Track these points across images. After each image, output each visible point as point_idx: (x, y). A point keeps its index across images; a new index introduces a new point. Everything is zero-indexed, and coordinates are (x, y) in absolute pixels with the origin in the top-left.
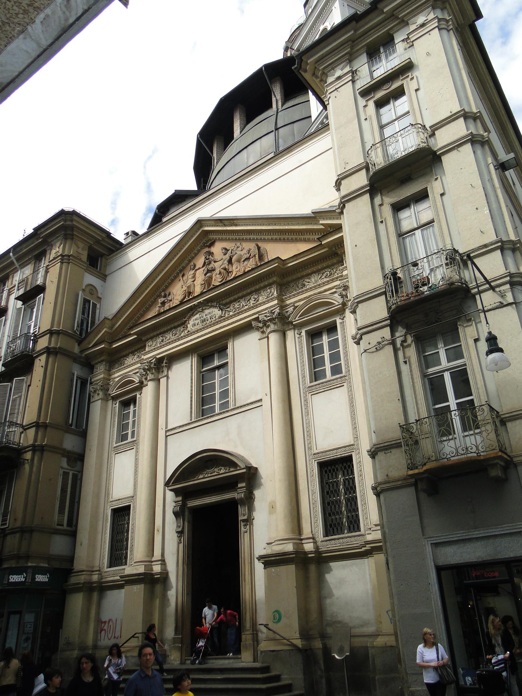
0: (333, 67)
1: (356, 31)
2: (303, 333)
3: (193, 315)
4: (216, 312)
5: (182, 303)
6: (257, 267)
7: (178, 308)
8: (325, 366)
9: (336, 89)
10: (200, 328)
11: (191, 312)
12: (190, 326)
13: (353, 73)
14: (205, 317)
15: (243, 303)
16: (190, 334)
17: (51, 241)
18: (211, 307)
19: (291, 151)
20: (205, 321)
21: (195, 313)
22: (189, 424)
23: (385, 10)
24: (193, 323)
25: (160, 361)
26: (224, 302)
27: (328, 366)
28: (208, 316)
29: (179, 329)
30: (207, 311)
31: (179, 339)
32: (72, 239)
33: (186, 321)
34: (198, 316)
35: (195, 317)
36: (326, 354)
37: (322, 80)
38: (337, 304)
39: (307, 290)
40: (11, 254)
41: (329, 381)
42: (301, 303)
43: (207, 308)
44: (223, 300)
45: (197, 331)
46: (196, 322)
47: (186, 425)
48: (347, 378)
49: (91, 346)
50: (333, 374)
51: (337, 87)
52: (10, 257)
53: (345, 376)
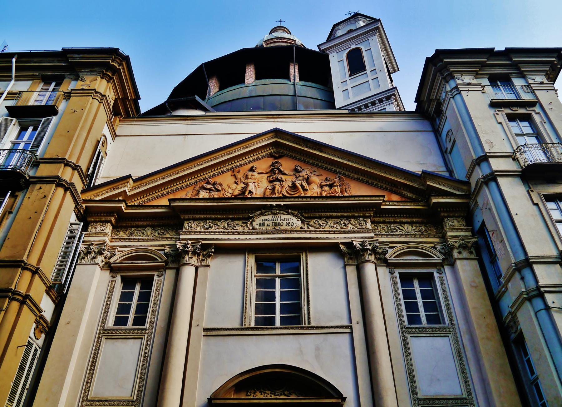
0: (463, 74)
1: (488, 60)
2: (397, 274)
3: (262, 214)
4: (296, 223)
5: (236, 198)
6: (191, 199)
7: (223, 201)
8: (129, 314)
9: (469, 90)
10: (265, 231)
11: (263, 211)
12: (256, 224)
13: (528, 86)
14: (279, 221)
15: (331, 222)
16: (254, 231)
17: (81, 72)
18: (293, 214)
19: (372, 117)
20: (279, 225)
21: (267, 213)
22: (237, 329)
23: (514, 59)
24: (261, 222)
25: (205, 247)
26: (306, 215)
27: (131, 316)
28: (285, 222)
29: (237, 222)
30: (283, 217)
31: (233, 233)
32: (108, 82)
33: (253, 217)
34: (270, 217)
35: (267, 217)
36: (420, 301)
37: (444, 78)
38: (160, 261)
39: (397, 235)
40: (14, 60)
41: (424, 328)
42: (399, 245)
43: (285, 213)
44: (305, 213)
45: (262, 232)
46: (267, 223)
47: (233, 329)
48: (451, 330)
49: (98, 198)
50: (134, 324)
51: (470, 89)
52: (11, 62)
53: (146, 329)
